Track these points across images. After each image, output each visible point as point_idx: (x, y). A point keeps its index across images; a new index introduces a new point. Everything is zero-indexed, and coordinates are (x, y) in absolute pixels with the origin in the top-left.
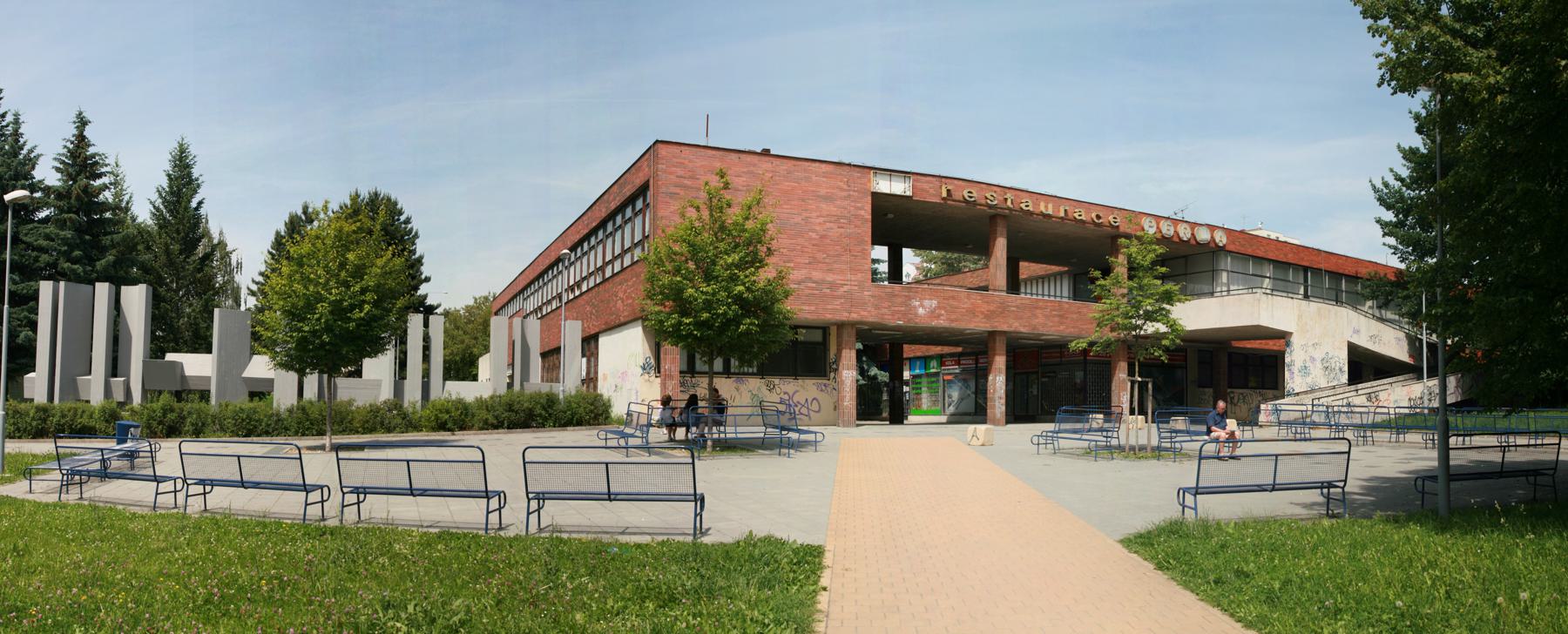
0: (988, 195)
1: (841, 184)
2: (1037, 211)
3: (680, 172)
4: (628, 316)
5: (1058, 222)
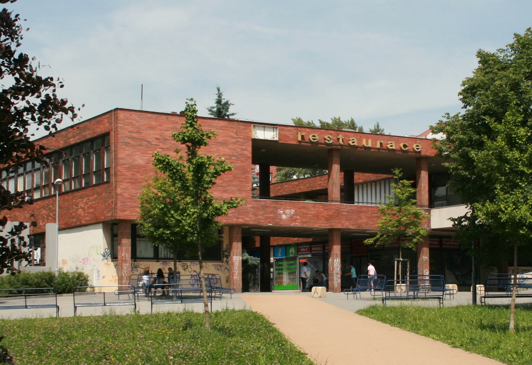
0: (326, 137)
1: (232, 134)
2: (360, 145)
3: (130, 128)
4: (89, 220)
5: (376, 151)
